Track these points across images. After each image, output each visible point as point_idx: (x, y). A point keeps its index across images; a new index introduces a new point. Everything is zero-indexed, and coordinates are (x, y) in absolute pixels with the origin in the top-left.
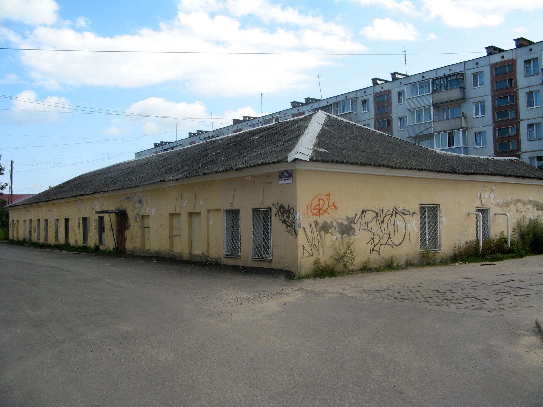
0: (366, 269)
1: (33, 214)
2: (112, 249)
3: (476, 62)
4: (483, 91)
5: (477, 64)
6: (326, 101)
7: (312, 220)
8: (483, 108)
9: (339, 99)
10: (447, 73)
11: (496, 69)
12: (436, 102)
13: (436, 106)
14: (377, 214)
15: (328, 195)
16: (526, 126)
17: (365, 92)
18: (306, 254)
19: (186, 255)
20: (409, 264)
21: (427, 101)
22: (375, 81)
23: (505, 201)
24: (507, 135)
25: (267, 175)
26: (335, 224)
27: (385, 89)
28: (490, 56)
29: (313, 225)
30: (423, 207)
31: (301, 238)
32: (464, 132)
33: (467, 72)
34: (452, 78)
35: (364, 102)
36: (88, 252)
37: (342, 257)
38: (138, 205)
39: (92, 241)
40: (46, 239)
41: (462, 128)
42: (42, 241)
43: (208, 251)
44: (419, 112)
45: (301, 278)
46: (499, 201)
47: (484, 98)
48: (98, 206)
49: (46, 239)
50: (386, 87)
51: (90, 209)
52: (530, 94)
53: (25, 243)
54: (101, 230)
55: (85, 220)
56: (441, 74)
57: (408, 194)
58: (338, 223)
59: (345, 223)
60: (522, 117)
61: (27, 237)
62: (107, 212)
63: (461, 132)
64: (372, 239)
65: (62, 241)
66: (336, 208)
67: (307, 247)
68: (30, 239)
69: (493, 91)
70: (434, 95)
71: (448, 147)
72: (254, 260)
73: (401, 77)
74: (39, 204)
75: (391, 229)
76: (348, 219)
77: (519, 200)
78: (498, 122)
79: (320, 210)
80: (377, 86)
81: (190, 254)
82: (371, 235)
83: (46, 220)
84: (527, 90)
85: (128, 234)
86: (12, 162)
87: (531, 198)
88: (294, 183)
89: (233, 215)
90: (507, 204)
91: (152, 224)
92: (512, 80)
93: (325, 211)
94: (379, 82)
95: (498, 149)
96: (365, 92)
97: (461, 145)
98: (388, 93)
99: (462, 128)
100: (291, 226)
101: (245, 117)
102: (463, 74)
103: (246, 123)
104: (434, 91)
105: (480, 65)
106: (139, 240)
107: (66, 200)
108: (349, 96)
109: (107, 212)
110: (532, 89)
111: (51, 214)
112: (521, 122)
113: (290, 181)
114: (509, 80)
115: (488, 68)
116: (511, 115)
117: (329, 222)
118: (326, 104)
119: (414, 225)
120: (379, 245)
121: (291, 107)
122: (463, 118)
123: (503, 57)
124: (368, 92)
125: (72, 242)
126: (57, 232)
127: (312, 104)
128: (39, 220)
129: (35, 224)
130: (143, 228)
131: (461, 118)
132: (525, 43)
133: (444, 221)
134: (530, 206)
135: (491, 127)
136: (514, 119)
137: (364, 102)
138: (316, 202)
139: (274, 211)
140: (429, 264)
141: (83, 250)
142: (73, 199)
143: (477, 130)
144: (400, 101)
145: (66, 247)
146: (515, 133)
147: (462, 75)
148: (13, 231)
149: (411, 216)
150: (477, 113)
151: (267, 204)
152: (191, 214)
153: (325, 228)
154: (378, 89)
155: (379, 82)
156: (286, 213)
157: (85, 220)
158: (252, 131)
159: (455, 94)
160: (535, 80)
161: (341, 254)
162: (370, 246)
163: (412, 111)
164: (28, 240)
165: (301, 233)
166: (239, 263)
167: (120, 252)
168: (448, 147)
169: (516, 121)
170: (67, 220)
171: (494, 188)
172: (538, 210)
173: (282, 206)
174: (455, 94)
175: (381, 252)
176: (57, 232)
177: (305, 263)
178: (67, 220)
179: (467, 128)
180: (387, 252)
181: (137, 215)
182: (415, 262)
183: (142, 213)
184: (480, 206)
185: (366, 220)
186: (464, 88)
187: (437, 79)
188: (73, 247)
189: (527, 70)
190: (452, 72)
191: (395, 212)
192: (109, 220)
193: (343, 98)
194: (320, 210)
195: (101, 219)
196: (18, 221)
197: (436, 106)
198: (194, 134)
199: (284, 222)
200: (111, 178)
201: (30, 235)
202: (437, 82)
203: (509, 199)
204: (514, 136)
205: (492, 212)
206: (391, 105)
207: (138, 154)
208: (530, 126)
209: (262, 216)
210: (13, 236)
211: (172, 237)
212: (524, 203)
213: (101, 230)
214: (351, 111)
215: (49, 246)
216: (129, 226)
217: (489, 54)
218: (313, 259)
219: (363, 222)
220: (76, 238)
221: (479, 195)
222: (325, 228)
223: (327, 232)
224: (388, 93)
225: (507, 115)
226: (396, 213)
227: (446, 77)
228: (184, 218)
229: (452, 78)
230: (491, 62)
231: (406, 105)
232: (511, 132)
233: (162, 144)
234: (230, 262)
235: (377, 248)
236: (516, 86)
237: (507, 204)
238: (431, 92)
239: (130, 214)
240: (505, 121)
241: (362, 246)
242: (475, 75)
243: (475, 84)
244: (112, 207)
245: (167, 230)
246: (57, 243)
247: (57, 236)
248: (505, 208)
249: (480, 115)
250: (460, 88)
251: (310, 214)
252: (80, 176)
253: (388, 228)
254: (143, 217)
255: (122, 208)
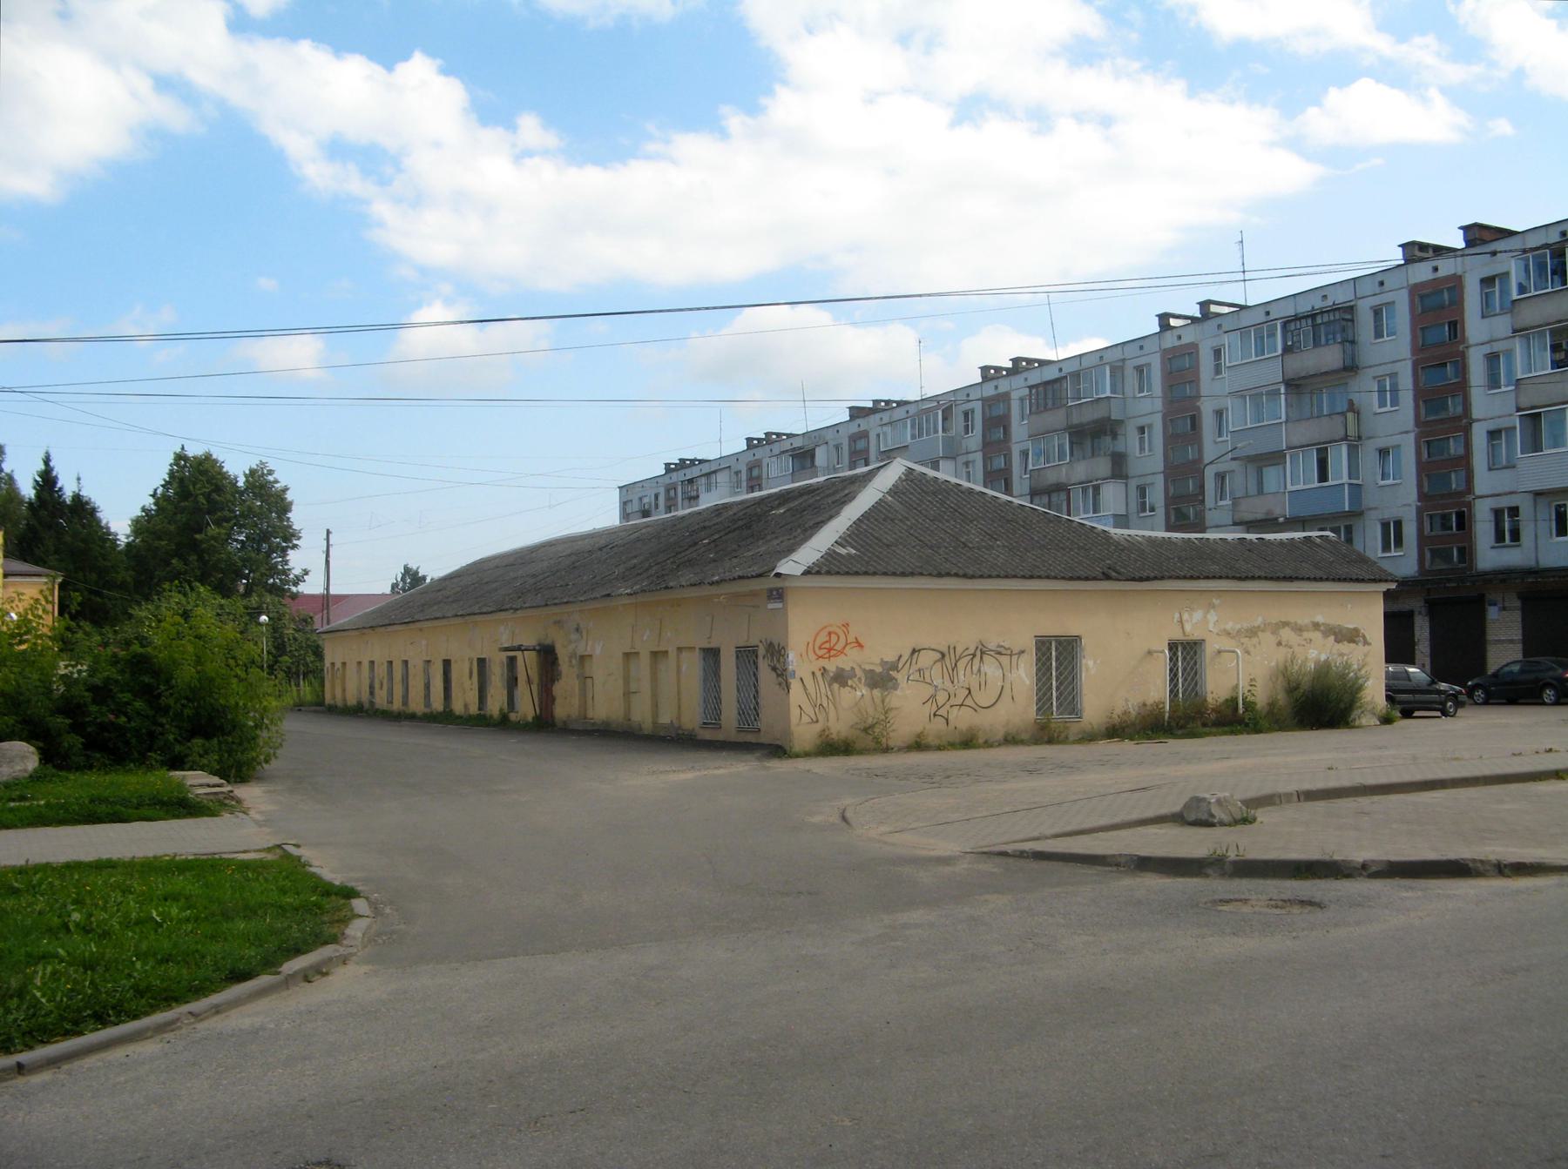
0: (918, 745)
1: (377, 650)
2: (530, 719)
3: (1380, 279)
4: (1391, 352)
5: (1382, 283)
6: (1262, 311)
7: (816, 665)
8: (1395, 390)
9: (1085, 364)
10: (1319, 304)
11: (1422, 297)
12: (1290, 375)
13: (1294, 385)
14: (943, 655)
15: (846, 625)
16: (1484, 436)
17: (1141, 348)
18: (805, 719)
19: (647, 727)
20: (1010, 740)
21: (1272, 373)
22: (1164, 318)
23: (1245, 625)
24: (1445, 456)
25: (754, 594)
26: (859, 673)
27: (1185, 340)
28: (1410, 267)
29: (818, 674)
30: (1043, 644)
31: (796, 694)
32: (1353, 451)
33: (1360, 303)
34: (1326, 318)
35: (1139, 370)
36: (488, 725)
37: (872, 726)
38: (574, 636)
39: (496, 703)
40: (405, 703)
41: (1345, 438)
42: (397, 705)
43: (679, 717)
44: (1257, 397)
45: (797, 756)
46: (1229, 626)
47: (1397, 367)
48: (504, 637)
49: (405, 703)
50: (1447, 267)
51: (493, 638)
52: (1492, 358)
53: (359, 712)
54: (512, 682)
55: (482, 662)
56: (1304, 307)
57: (1013, 621)
58: (864, 670)
59: (879, 669)
60: (1476, 414)
61: (365, 697)
62: (519, 648)
63: (1344, 449)
64: (933, 696)
65: (438, 705)
66: (860, 646)
67: (804, 707)
68: (372, 703)
69: (1416, 350)
70: (1288, 358)
71: (1317, 484)
72: (740, 730)
73: (1226, 310)
74: (390, 629)
75: (974, 682)
76: (883, 663)
77: (1285, 624)
78: (1427, 423)
79: (830, 650)
80: (1168, 334)
81: (655, 723)
82: (931, 690)
83: (406, 663)
84: (1487, 349)
85: (558, 689)
86: (328, 532)
87: (1319, 619)
88: (785, 609)
89: (712, 655)
90: (1252, 632)
91: (597, 671)
92: (1456, 327)
93: (841, 652)
94: (1173, 322)
95: (1426, 489)
96: (1141, 348)
97: (1345, 479)
98: (1191, 350)
99: (1345, 438)
100: (782, 675)
101: (876, 402)
102: (1351, 309)
103: (878, 416)
104: (1287, 350)
105: (1387, 286)
106: (576, 701)
107: (444, 622)
108: (1108, 357)
109: (519, 648)
110: (1497, 347)
111: (416, 650)
112: (1475, 425)
113: (780, 605)
114: (1450, 323)
115: (1404, 295)
116: (1454, 407)
117: (848, 668)
118: (1056, 375)
119: (1024, 674)
120: (947, 706)
121: (980, 380)
122: (1350, 416)
123: (1436, 269)
124: (1145, 343)
125: (457, 707)
126: (427, 687)
127: (1025, 375)
128: (390, 663)
129: (381, 671)
130: (584, 678)
131: (1343, 414)
132: (1487, 236)
133: (1090, 666)
134: (1316, 636)
135: (1411, 437)
136: (1459, 418)
137: (1139, 370)
138: (823, 638)
139: (761, 651)
140: (1050, 741)
141: (479, 722)
142: (459, 620)
143: (1382, 443)
144: (1218, 370)
145: (446, 719)
146: (1461, 451)
147: (1348, 311)
148: (333, 687)
149: (1015, 658)
150: (1382, 404)
151: (753, 642)
152: (654, 654)
153: (841, 678)
154: (1170, 341)
155: (1173, 322)
156: (777, 652)
157: (482, 662)
158: (789, 492)
159: (1330, 357)
160: (1502, 325)
161: (870, 721)
162: (929, 709)
163: (1239, 394)
164: (367, 706)
165: (795, 685)
166: (720, 736)
167: (545, 725)
168: (1317, 484)
169: (1463, 423)
170: (447, 664)
171: (1216, 602)
172: (1338, 641)
173: (771, 644)
174: (1330, 357)
175: (951, 718)
176: (427, 687)
177: (803, 732)
178: (447, 664)
179: (1360, 438)
180: (963, 719)
181: (573, 655)
182: (1025, 736)
183: (581, 651)
184: (1177, 635)
185: (919, 665)
186: (1353, 342)
187: (1297, 318)
188: (460, 717)
189: (1487, 301)
190: (1329, 302)
191: (982, 651)
192: (528, 663)
193: (1095, 360)
194: (830, 650)
195: (512, 660)
196: (344, 664)
197: (1294, 385)
198: (759, 440)
199: (774, 669)
200: (534, 576)
201: (372, 693)
202: (1292, 326)
203: (1259, 621)
204: (1460, 457)
205: (1210, 649)
206: (1198, 380)
207: (627, 491)
208: (1494, 435)
209: (747, 655)
210: (334, 697)
211: (628, 694)
212: (1299, 629)
213: (512, 682)
214: (1108, 394)
215: (412, 717)
216: (560, 674)
217: (1470, 243)
218: (818, 727)
219: (915, 667)
220: (465, 699)
221: (1177, 615)
222: (841, 678)
223: (844, 684)
224: (1191, 350)
225: (1445, 408)
226: (982, 653)
227: (1312, 316)
228: (645, 660)
229: (1326, 318)
230: (1413, 281)
231: (1227, 382)
232: (1455, 448)
233: (683, 464)
234: (707, 735)
235: (942, 712)
236: (1464, 340)
237: (1252, 632)
238: (1280, 352)
239: (562, 653)
240: (1442, 421)
241: (910, 707)
242: (1377, 312)
243: (1378, 334)
244: (529, 639)
245: (621, 682)
246: (427, 710)
247: (427, 696)
248: (1245, 640)
249: (1389, 408)
250: (1342, 343)
251: (812, 657)
252: (475, 564)
253: (962, 676)
254: (582, 658)
255: (548, 642)
